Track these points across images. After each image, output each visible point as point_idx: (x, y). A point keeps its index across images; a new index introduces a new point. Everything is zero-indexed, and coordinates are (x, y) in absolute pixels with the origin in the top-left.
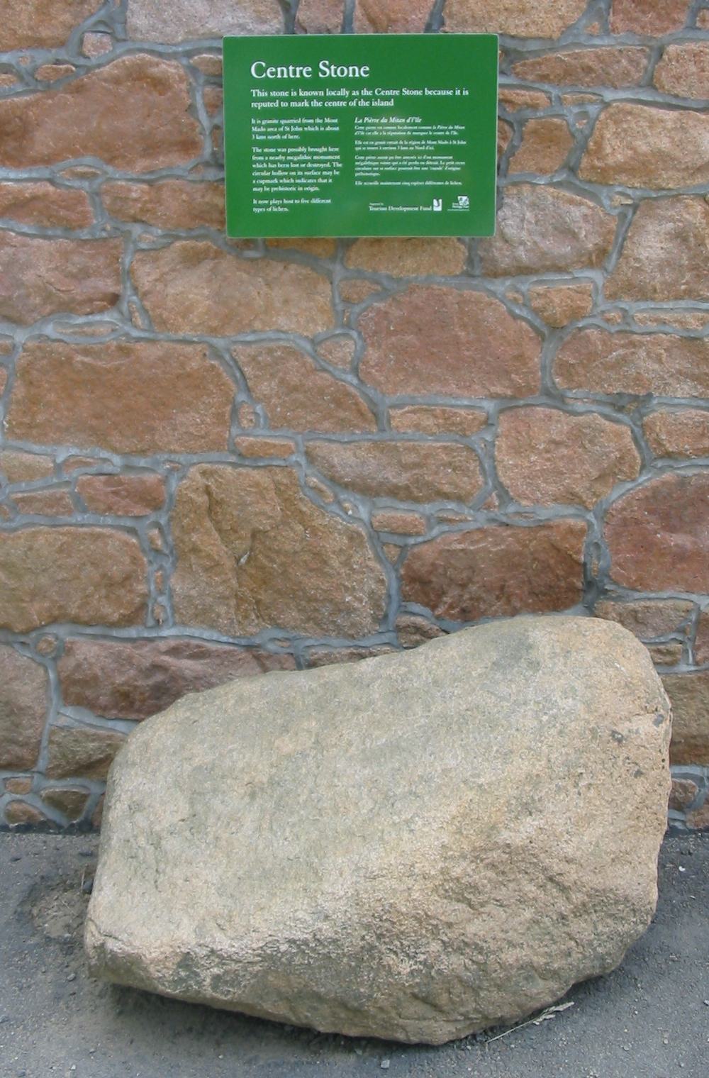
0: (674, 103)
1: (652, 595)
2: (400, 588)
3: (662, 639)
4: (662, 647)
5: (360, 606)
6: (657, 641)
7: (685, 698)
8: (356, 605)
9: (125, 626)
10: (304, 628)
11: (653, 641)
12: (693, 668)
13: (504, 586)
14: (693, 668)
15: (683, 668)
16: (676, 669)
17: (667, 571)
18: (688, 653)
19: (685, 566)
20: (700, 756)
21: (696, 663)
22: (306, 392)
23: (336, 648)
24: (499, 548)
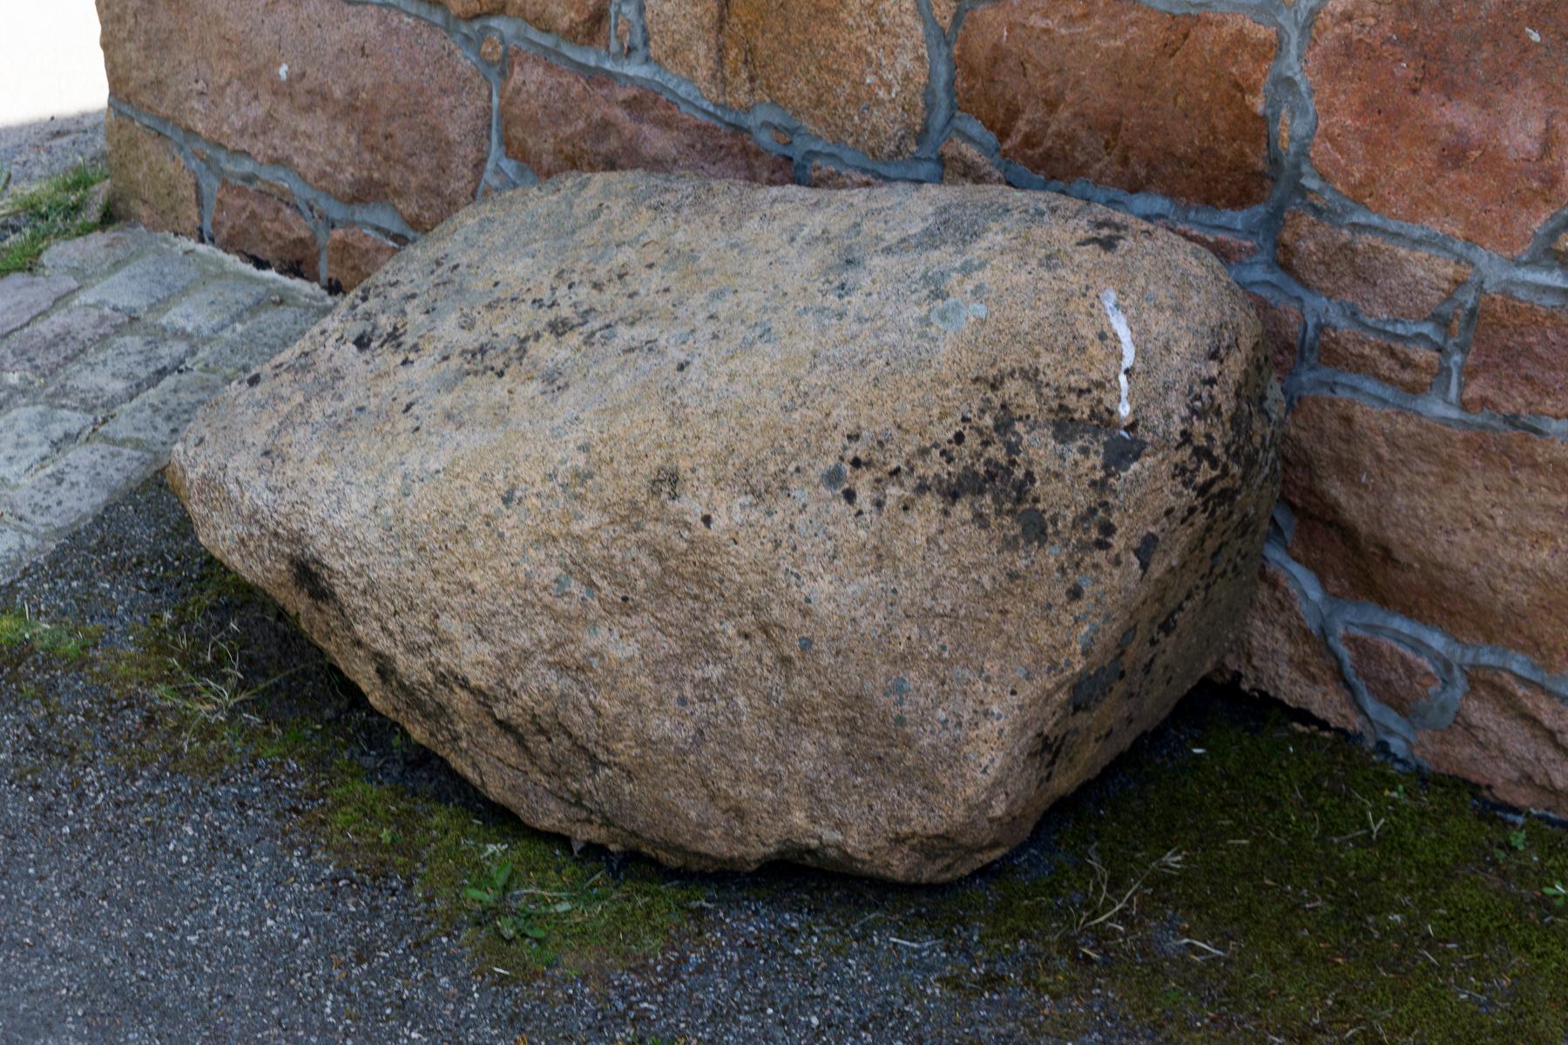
0: (1437, 636)
1: (1393, 226)
2: (951, 82)
3: (1400, 329)
4: (1398, 347)
5: (886, 98)
6: (1389, 328)
7: (1432, 473)
8: (882, 94)
9: (582, 44)
10: (812, 116)
11: (1380, 326)
12: (1454, 414)
13: (1120, 124)
14: (1454, 414)
15: (1437, 408)
16: (1420, 404)
17: (612, 222)
18: (1449, 376)
19: (315, 636)
20: (1451, 614)
21: (1464, 406)
22: (1434, 141)
23: (847, 166)
24: (1112, 42)
